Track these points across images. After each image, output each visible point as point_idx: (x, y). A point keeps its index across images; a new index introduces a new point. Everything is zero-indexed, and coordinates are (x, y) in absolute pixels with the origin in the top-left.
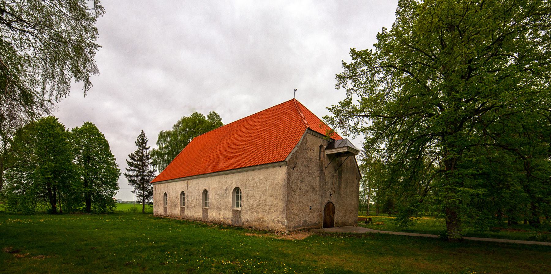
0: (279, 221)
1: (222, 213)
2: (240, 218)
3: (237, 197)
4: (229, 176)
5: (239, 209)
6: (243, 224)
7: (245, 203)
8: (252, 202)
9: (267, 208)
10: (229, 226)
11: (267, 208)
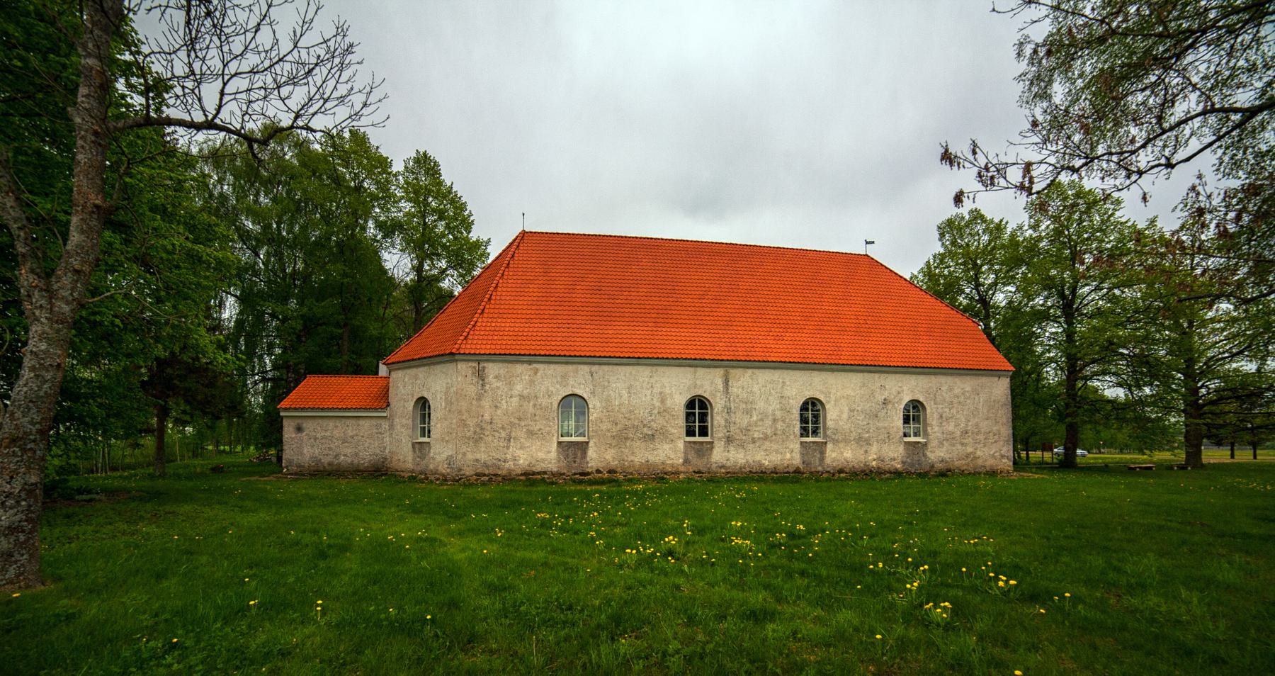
0: (1003, 456)
1: (874, 448)
2: (925, 455)
3: (423, 417)
4: (791, 372)
5: (426, 439)
6: (933, 466)
7: (936, 429)
8: (951, 427)
9: (981, 437)
10: (897, 474)
11: (981, 437)
